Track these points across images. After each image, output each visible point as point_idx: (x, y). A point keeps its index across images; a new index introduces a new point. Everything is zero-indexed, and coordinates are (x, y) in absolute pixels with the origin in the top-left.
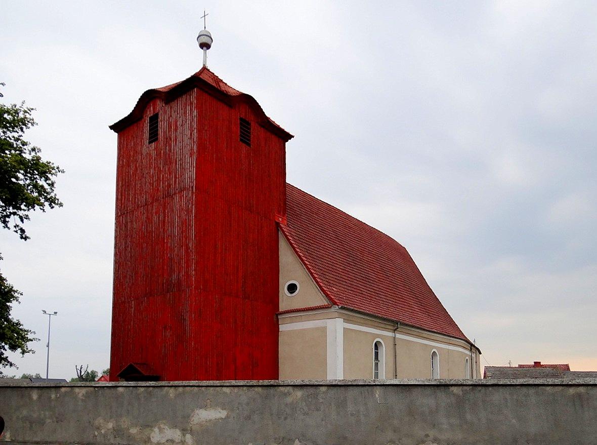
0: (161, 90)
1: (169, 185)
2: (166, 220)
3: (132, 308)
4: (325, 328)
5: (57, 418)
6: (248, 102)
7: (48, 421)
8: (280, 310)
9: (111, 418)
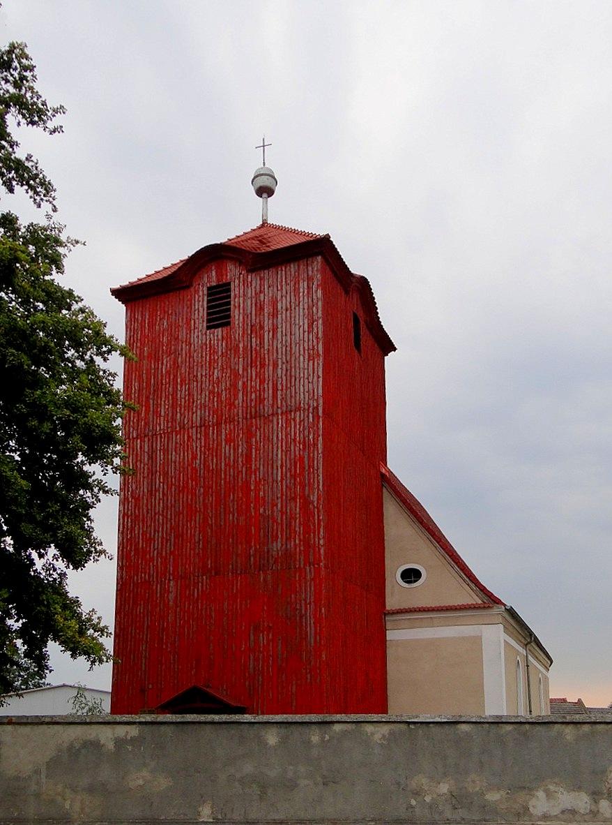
0: (247, 246)
1: (261, 400)
2: (254, 454)
3: (169, 592)
4: (480, 638)
5: (324, 777)
6: (363, 286)
7: (303, 782)
8: (388, 608)
9: (445, 775)
